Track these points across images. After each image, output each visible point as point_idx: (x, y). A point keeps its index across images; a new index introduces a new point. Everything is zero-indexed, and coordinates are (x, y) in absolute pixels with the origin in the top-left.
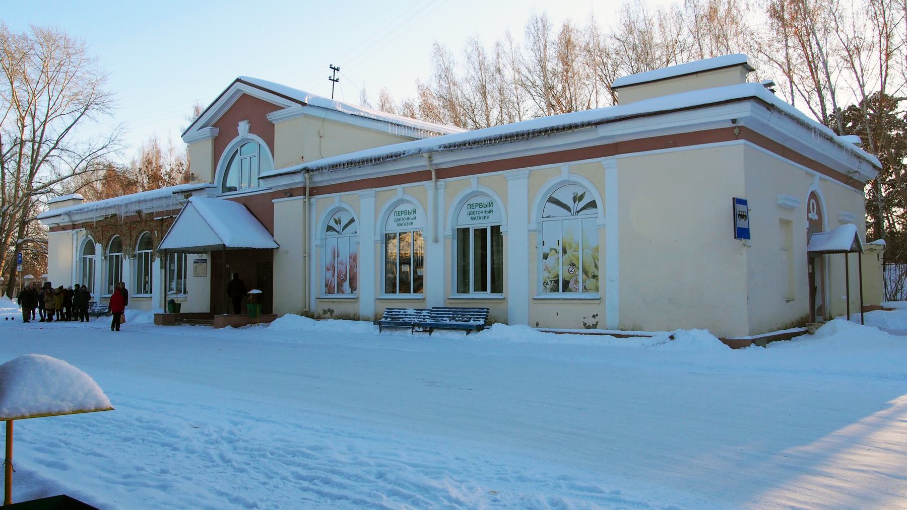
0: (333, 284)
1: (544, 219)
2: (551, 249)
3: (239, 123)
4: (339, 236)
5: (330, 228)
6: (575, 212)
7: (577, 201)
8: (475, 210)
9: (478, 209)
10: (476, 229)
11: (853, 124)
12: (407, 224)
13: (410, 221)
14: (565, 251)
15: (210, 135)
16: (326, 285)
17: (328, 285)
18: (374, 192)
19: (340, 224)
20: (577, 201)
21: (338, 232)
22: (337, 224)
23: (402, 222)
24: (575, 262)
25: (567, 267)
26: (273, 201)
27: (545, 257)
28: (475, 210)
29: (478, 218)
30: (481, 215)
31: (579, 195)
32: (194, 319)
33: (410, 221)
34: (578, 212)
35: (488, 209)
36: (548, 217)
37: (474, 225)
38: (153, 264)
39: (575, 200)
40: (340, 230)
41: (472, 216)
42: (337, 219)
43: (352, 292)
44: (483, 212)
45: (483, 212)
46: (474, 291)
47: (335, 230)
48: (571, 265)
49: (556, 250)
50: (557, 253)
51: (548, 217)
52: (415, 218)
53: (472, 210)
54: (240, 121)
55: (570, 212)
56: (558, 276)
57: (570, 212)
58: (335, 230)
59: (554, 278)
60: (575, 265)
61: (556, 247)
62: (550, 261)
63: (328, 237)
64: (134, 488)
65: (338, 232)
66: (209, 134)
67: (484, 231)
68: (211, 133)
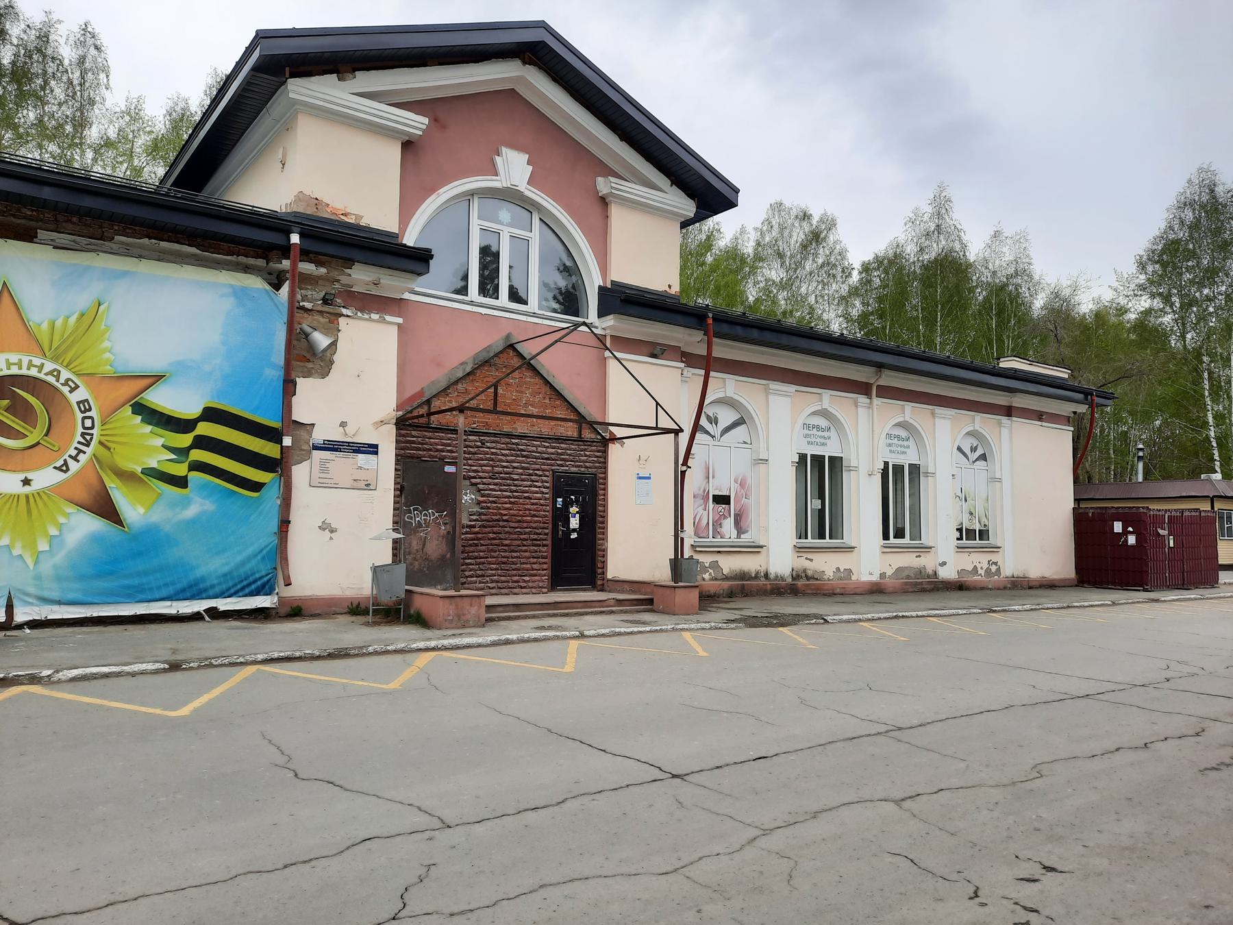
10: (888, 465)
12: (819, 444)
13: (903, 449)
15: (424, 127)
19: (716, 425)
21: (713, 437)
22: (712, 424)
33: (903, 449)
37: (810, 451)
38: (229, 69)
40: (718, 435)
42: (712, 416)
43: (738, 537)
44: (901, 446)
45: (901, 446)
53: (809, 432)
56: (962, 523)
58: (707, 433)
64: (62, 359)
65: (713, 437)
66: (419, 129)
67: (898, 469)
68: (424, 131)
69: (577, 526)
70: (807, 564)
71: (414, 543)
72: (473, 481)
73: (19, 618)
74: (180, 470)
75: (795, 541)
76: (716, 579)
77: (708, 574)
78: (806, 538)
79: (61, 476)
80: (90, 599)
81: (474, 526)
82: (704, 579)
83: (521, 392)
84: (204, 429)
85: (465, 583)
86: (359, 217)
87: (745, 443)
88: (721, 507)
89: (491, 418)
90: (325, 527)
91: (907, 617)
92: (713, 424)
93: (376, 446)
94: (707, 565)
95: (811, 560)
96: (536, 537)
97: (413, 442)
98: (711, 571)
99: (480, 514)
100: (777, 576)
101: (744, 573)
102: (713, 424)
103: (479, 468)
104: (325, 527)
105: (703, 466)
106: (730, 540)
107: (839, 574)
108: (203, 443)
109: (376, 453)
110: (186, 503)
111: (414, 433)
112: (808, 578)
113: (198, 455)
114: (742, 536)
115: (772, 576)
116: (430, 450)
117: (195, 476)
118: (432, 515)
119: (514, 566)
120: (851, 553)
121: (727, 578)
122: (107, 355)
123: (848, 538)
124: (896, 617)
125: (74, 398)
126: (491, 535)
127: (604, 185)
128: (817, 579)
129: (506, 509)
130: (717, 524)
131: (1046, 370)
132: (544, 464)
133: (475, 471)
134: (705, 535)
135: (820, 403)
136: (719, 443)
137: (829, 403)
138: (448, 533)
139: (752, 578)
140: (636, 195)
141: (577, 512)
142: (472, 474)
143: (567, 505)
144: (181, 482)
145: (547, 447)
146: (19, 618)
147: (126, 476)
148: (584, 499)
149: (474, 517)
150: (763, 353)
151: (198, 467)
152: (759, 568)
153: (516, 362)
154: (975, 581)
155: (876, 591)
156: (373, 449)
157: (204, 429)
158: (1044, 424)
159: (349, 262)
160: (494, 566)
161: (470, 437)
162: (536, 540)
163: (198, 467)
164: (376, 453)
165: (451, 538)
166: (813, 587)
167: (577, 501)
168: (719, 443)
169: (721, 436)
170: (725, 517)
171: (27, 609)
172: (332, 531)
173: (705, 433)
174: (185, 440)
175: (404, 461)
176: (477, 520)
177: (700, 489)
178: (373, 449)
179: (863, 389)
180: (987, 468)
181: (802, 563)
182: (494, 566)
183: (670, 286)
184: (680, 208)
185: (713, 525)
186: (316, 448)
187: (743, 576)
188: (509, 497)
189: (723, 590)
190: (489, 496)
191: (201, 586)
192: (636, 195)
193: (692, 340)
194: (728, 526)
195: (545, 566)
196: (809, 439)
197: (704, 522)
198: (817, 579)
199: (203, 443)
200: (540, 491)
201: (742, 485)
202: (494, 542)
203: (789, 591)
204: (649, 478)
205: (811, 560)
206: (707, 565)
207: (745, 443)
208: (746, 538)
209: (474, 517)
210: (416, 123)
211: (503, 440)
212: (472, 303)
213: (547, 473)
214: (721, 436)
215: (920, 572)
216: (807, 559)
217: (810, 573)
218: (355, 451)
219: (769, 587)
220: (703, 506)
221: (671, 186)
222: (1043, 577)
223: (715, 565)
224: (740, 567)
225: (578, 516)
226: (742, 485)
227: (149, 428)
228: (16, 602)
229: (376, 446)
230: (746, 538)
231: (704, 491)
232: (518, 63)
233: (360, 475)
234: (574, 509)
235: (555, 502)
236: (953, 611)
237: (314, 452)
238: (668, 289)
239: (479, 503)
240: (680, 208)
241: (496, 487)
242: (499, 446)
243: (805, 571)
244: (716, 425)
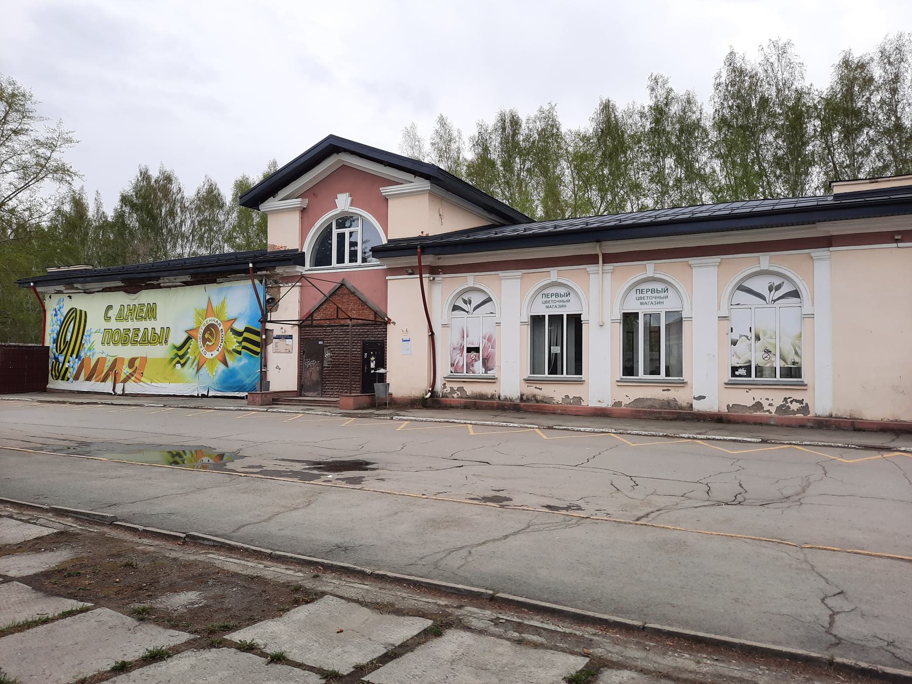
0: (461, 364)
1: (732, 307)
2: (741, 336)
3: (338, 195)
4: (469, 316)
5: (456, 308)
6: (770, 301)
7: (774, 291)
8: (550, 299)
9: (649, 294)
11: (902, 237)
14: (758, 338)
16: (452, 365)
17: (454, 364)
18: (521, 274)
19: (470, 304)
20: (774, 291)
21: (467, 312)
23: (551, 305)
24: (769, 348)
25: (761, 354)
26: (387, 278)
27: (734, 343)
28: (550, 299)
29: (650, 303)
30: (557, 304)
31: (776, 284)
32: (277, 399)
34: (775, 301)
35: (565, 299)
36: (738, 304)
39: (770, 289)
40: (471, 310)
41: (547, 305)
43: (486, 372)
44: (560, 301)
45: (560, 301)
46: (660, 374)
47: (464, 310)
48: (765, 352)
49: (747, 337)
50: (748, 339)
51: (738, 304)
52: (81, 311)
53: (548, 299)
54: (338, 193)
55: (765, 300)
57: (765, 300)
59: (746, 363)
60: (770, 352)
61: (748, 334)
62: (742, 345)
63: (753, 312)
65: (467, 312)
69: (374, 367)
70: (537, 392)
71: (308, 374)
72: (329, 347)
73: (210, 395)
74: (239, 349)
75: (527, 374)
76: (462, 398)
77: (456, 394)
78: (562, 374)
79: (218, 352)
80: (223, 390)
81: (329, 367)
82: (453, 397)
83: (348, 305)
84: (246, 335)
85: (326, 392)
86: (286, 247)
87: (492, 313)
88: (473, 354)
89: (337, 321)
90: (277, 367)
91: (455, 423)
92: (468, 304)
93: (292, 336)
94: (456, 389)
95: (541, 389)
96: (354, 372)
97: (307, 333)
98: (458, 392)
99: (332, 362)
100: (507, 398)
101: (482, 394)
102: (468, 304)
103: (331, 342)
104: (277, 367)
105: (461, 330)
106: (479, 375)
107: (568, 400)
108: (245, 340)
109: (292, 338)
110: (240, 360)
111: (307, 329)
112: (537, 401)
113: (244, 344)
114: (488, 372)
115: (502, 398)
116: (313, 335)
117: (243, 351)
118: (314, 362)
119: (345, 385)
120: (582, 385)
121: (469, 397)
122: (226, 314)
123: (685, 377)
124: (447, 421)
125: (220, 329)
126: (336, 371)
127: (387, 190)
128: (546, 402)
129: (342, 359)
130: (470, 365)
131: (903, 181)
132: (358, 337)
133: (329, 343)
134: (461, 372)
135: (759, 265)
136: (471, 316)
137: (770, 263)
138: (320, 370)
139: (489, 398)
140: (395, 191)
141: (374, 360)
142: (328, 344)
143: (369, 356)
144: (239, 353)
145: (359, 329)
146: (210, 395)
147: (229, 351)
148: (378, 353)
149: (329, 363)
150: (487, 256)
151: (244, 348)
152: (494, 392)
153: (346, 291)
154: (755, 417)
155: (600, 414)
156: (290, 337)
157: (246, 335)
158: (900, 245)
159: (274, 267)
160: (337, 385)
161: (328, 328)
162: (354, 373)
163: (244, 348)
164: (292, 338)
165: (321, 372)
166: (534, 408)
167: (374, 354)
168: (471, 316)
169: (474, 311)
170: (476, 361)
171: (212, 392)
172: (279, 369)
173: (462, 310)
174: (240, 339)
175: (302, 340)
176: (330, 364)
177: (458, 344)
178: (290, 337)
179: (592, 259)
180: (799, 305)
181: (530, 390)
182: (337, 385)
183: (422, 232)
184: (420, 188)
185: (467, 365)
186: (274, 338)
187: (482, 397)
188: (343, 354)
189: (461, 404)
190: (335, 353)
191: (245, 388)
192: (395, 191)
193: (412, 261)
194: (478, 367)
195: (358, 386)
196: (547, 305)
197: (461, 364)
198: (546, 402)
199: (245, 340)
200: (358, 349)
201: (489, 340)
202: (336, 374)
203: (512, 409)
204: (409, 341)
205: (541, 389)
206: (456, 389)
207: (492, 313)
208: (490, 373)
209: (329, 363)
210: (296, 202)
211: (340, 328)
212: (334, 268)
213: (360, 342)
214: (474, 311)
215: (668, 403)
216: (536, 388)
217: (539, 398)
218: (286, 338)
219: (495, 405)
220: (460, 354)
221: (415, 177)
222: (896, 421)
223: (461, 389)
224: (479, 391)
225: (374, 361)
226: (489, 340)
227: (233, 336)
228: (210, 390)
229: (292, 336)
230: (490, 373)
231: (461, 345)
232: (335, 155)
233: (287, 347)
234: (373, 358)
235: (364, 355)
236: (502, 423)
237: (274, 340)
238: (421, 234)
239: (331, 357)
240: (420, 188)
241: (338, 350)
242: (339, 331)
243: (534, 396)
244: (470, 304)
